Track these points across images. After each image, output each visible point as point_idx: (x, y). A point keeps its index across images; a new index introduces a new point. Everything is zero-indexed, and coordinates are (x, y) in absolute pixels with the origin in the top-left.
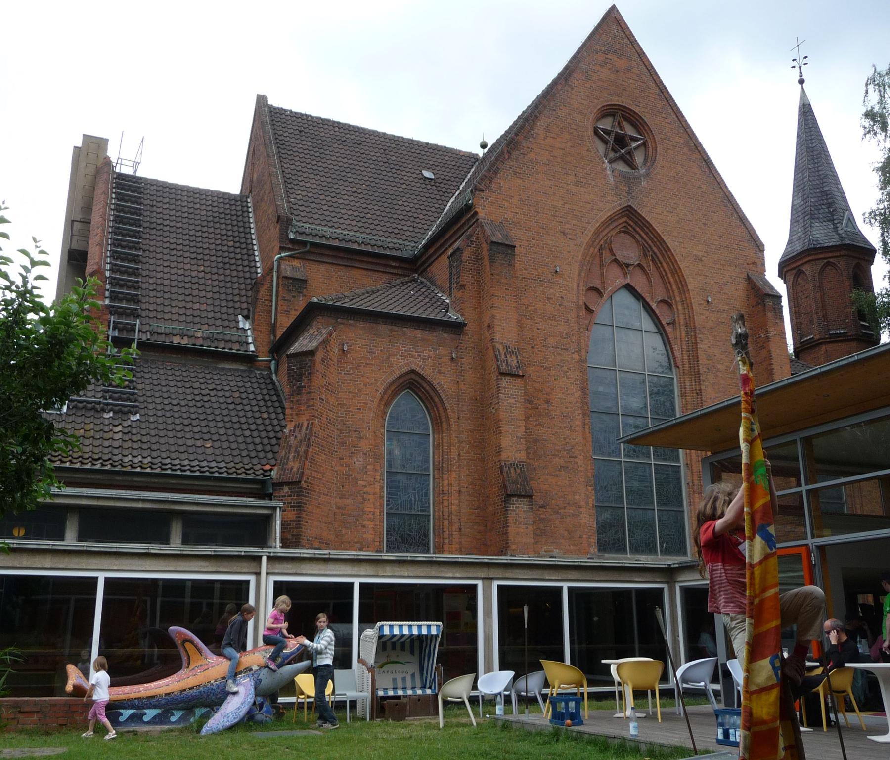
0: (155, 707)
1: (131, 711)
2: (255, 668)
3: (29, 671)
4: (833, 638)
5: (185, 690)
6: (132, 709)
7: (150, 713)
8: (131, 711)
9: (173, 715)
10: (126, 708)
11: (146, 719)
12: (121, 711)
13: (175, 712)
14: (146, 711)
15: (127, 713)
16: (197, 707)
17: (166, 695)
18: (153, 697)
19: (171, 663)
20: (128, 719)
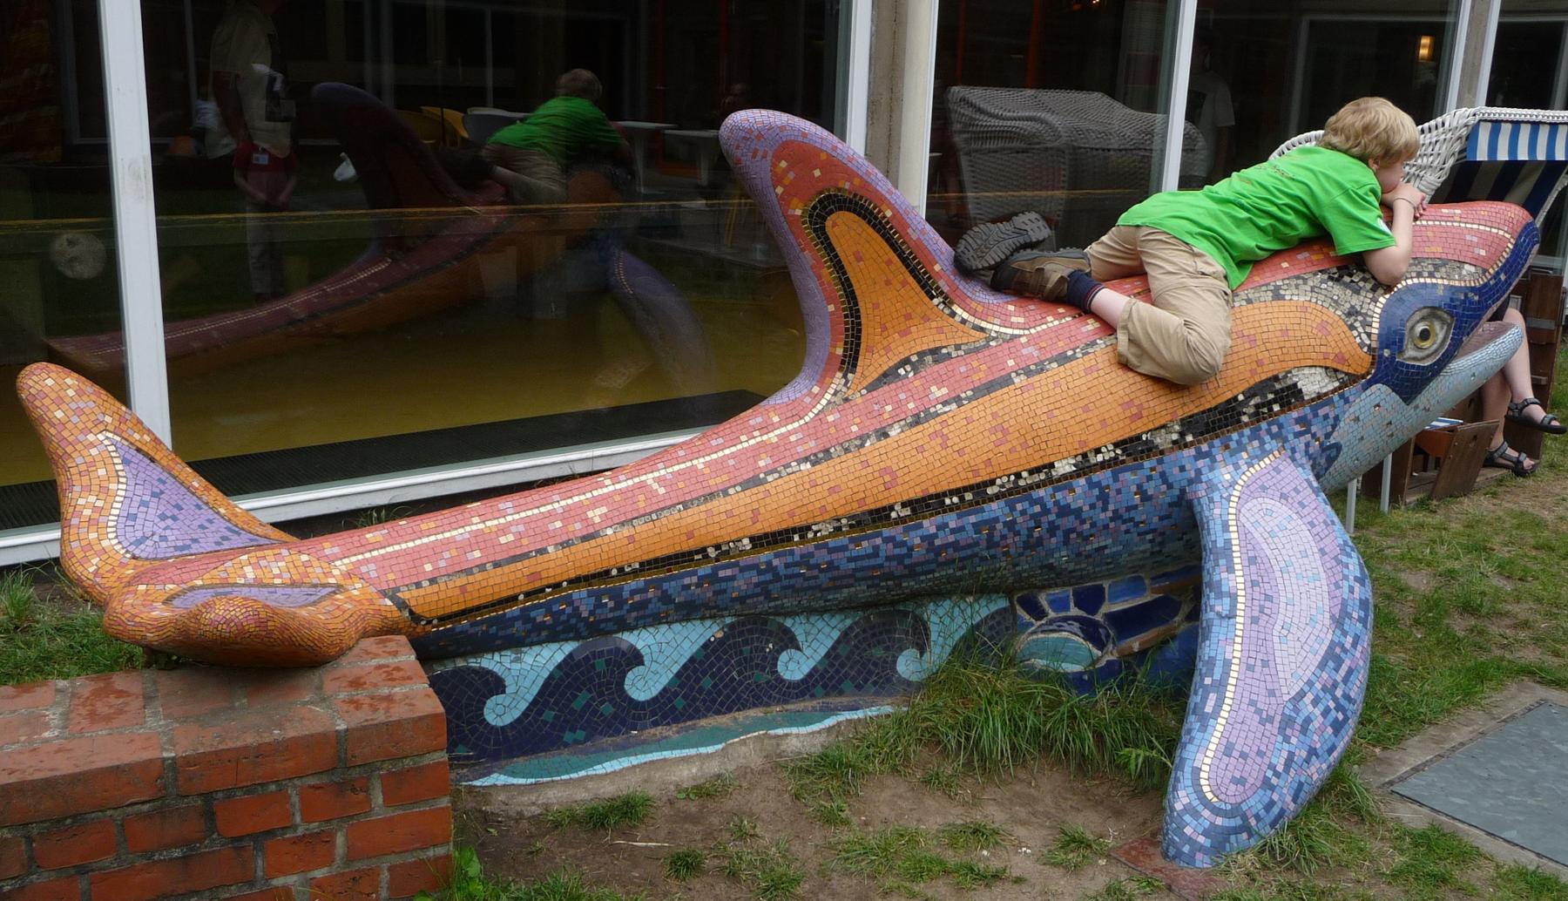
0: (689, 611)
1: (544, 659)
2: (1312, 383)
3: (1020, 119)
4: (358, 586)
5: (880, 516)
6: (554, 636)
7: (662, 653)
8: (544, 659)
9: (789, 641)
10: (516, 643)
11: (642, 686)
12: (490, 662)
13: (798, 627)
14: (640, 639)
15: (526, 671)
16: (937, 594)
17: (759, 541)
18: (682, 558)
19: (727, 302)
20: (537, 704)
